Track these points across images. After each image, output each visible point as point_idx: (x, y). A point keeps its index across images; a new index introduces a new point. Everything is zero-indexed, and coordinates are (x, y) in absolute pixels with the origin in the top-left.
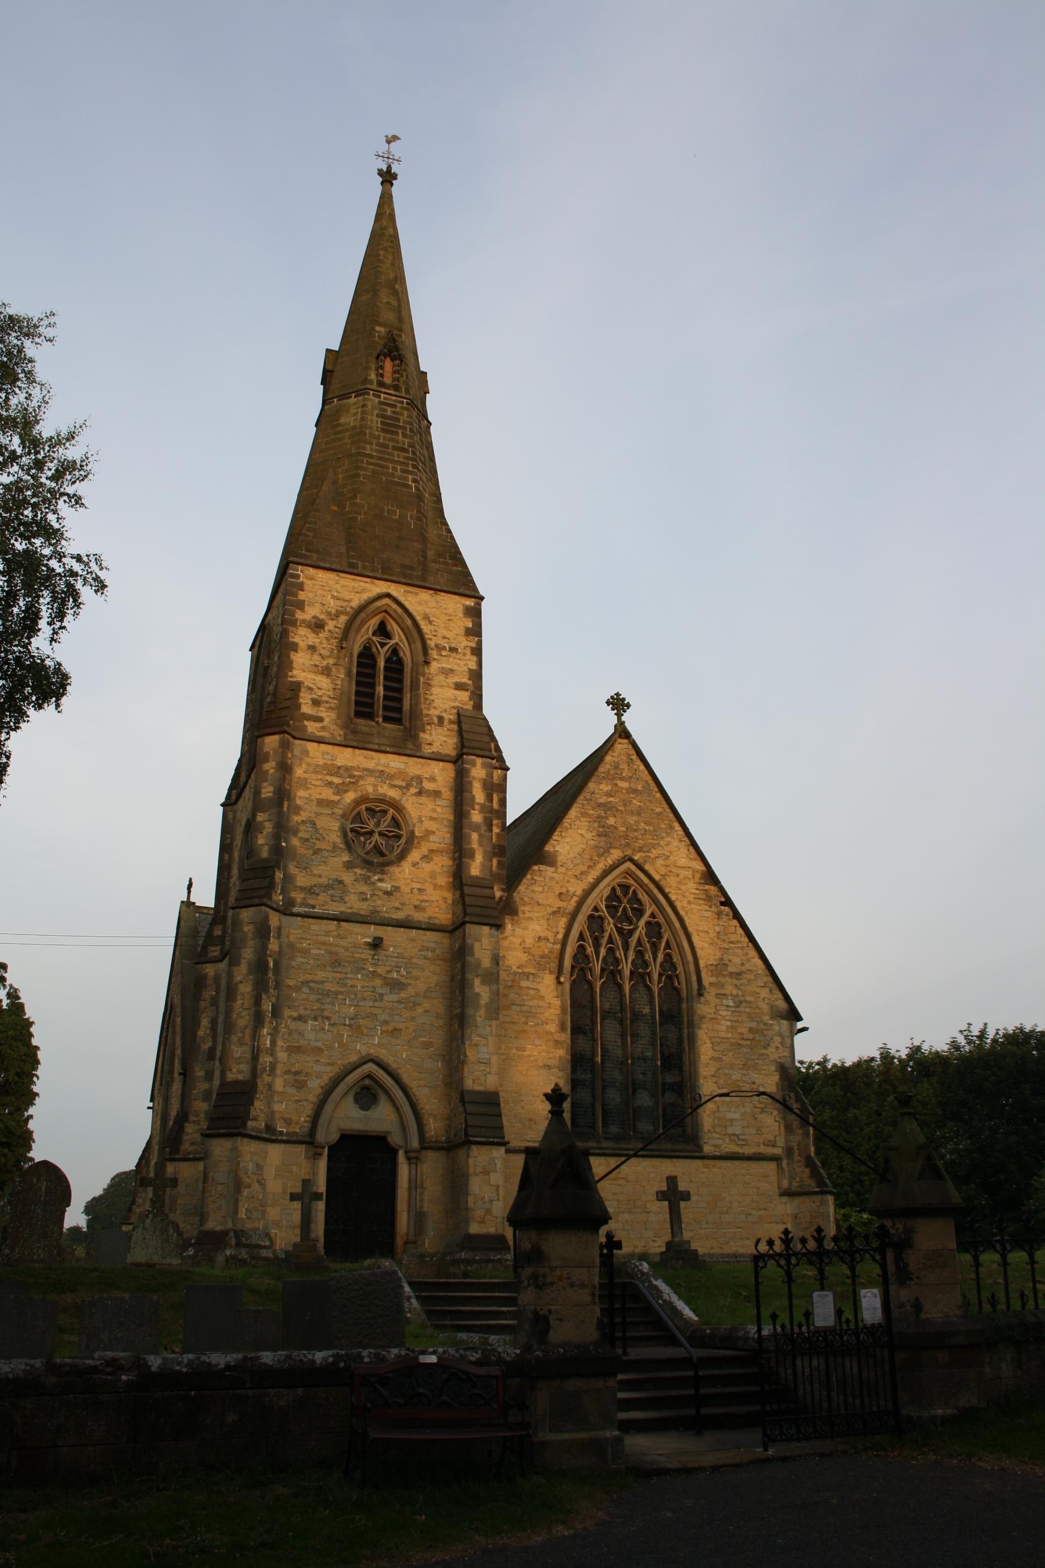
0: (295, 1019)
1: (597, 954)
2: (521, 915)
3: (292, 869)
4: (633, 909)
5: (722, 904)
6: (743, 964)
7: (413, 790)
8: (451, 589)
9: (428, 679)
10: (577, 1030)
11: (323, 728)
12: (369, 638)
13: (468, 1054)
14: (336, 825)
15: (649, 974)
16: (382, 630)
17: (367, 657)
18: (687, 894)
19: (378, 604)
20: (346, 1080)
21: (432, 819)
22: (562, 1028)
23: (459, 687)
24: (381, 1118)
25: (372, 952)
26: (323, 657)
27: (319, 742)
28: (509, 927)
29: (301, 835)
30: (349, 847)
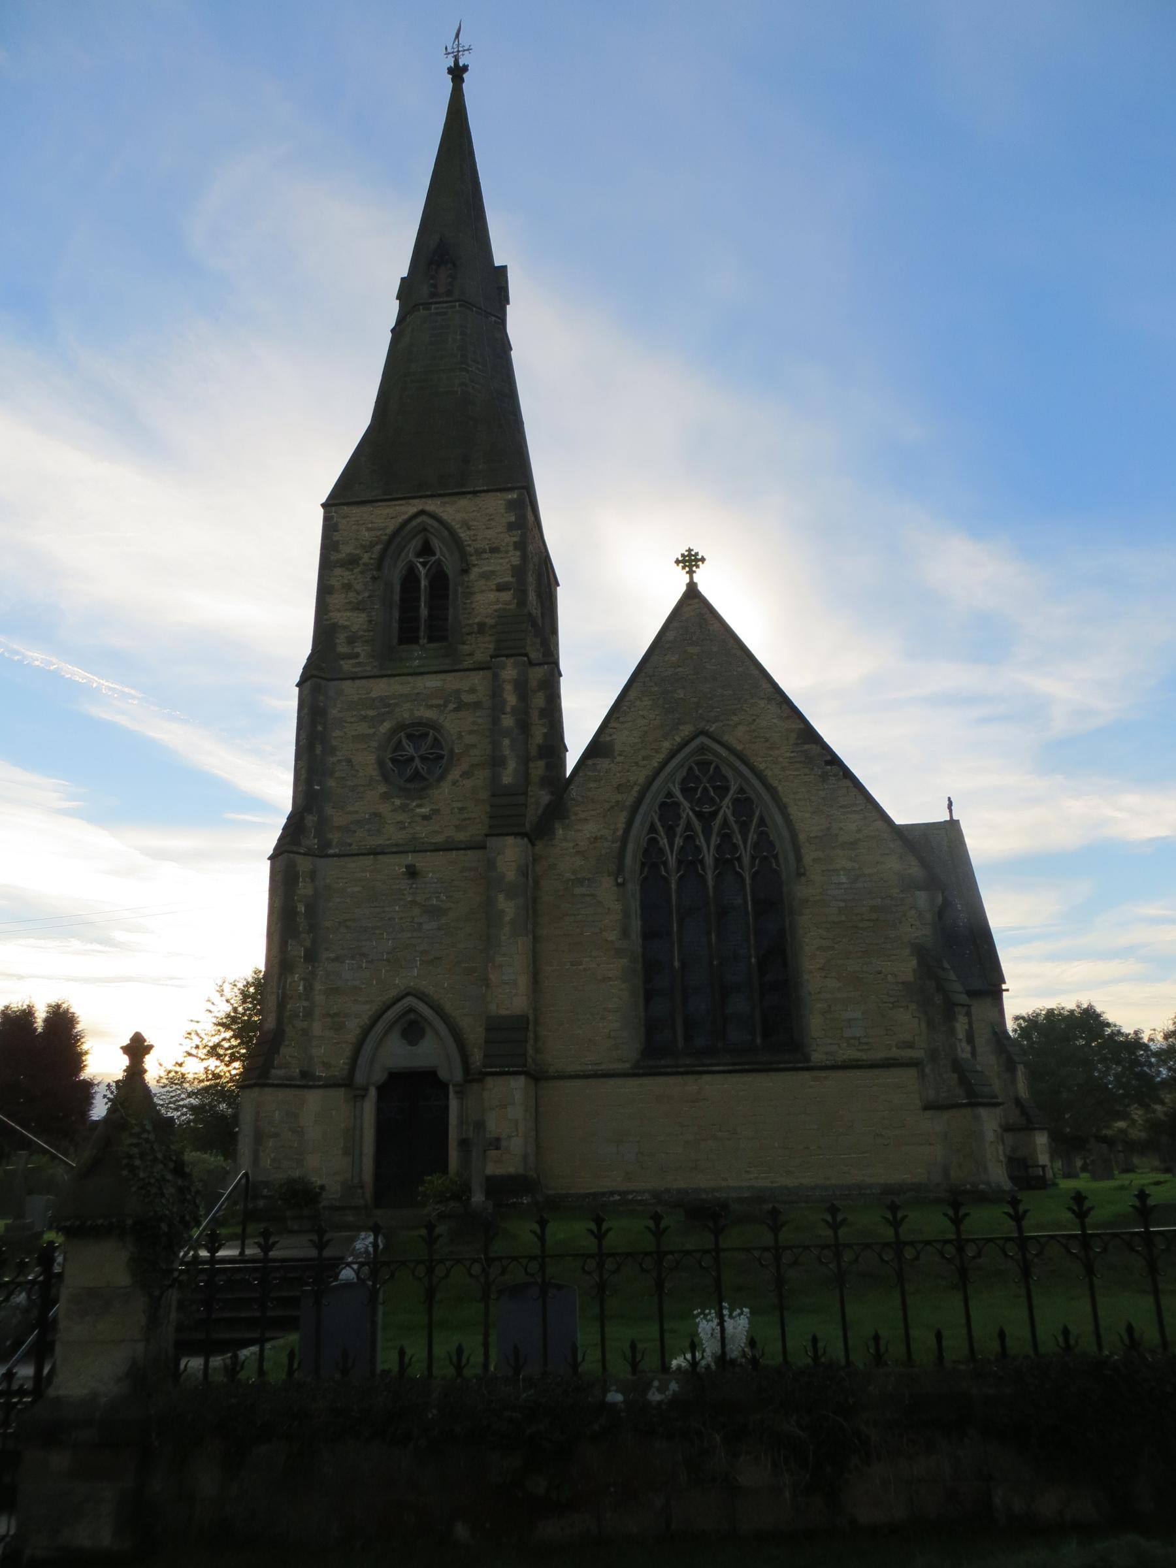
0: (333, 960)
1: (671, 845)
2: (573, 818)
3: (329, 810)
4: (715, 788)
5: (828, 763)
6: (859, 831)
7: (451, 706)
8: (491, 487)
9: (468, 587)
10: (649, 935)
11: (359, 664)
12: (434, 554)
13: (491, 976)
14: (372, 759)
15: (739, 859)
16: (426, 550)
17: (410, 578)
18: (780, 759)
19: (414, 523)
20: (385, 1016)
21: (471, 732)
22: (625, 933)
23: (501, 588)
24: (428, 1053)
25: (410, 881)
26: (358, 593)
27: (353, 679)
28: (560, 832)
29: (337, 774)
30: (386, 777)
